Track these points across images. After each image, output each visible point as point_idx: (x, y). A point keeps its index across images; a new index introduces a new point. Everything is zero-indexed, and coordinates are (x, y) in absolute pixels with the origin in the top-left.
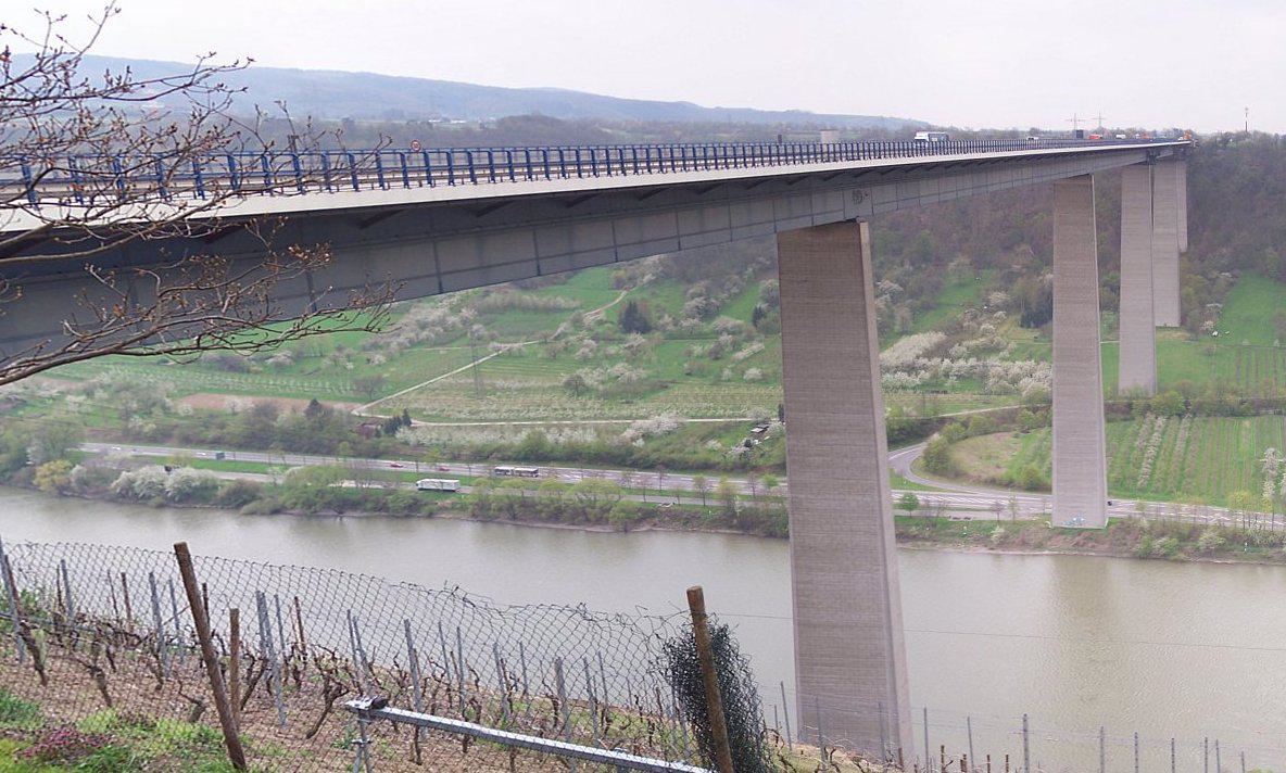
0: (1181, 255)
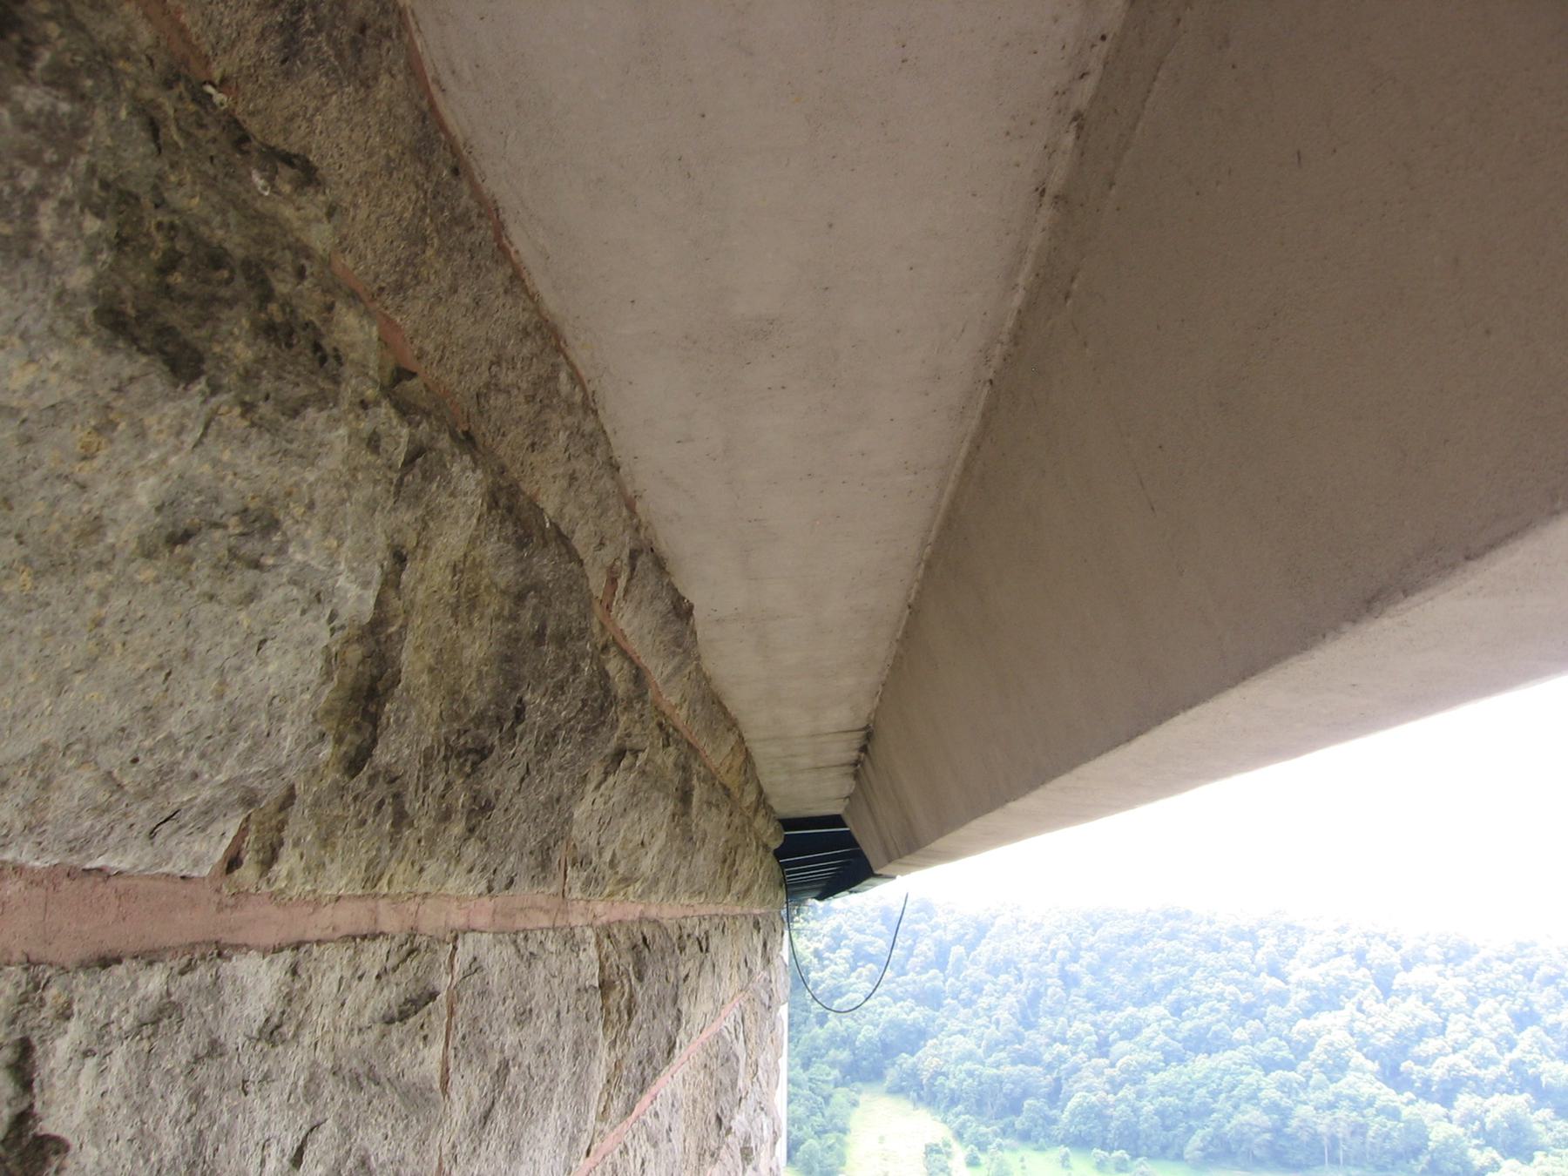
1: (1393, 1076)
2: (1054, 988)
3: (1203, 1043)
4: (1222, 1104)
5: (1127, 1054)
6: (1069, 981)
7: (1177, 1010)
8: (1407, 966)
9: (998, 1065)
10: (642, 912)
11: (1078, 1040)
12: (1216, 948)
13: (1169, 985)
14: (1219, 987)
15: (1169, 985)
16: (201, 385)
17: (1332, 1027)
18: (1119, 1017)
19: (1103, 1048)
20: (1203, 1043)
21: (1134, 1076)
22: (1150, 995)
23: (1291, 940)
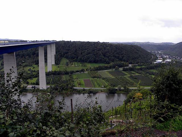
0: (55, 55)
1: (104, 56)
5: (83, 54)
19: (81, 54)
21: (84, 56)
22: (86, 49)
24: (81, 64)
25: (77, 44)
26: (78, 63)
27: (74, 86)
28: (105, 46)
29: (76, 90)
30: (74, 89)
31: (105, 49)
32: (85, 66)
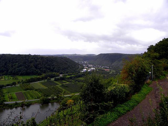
1: (36, 68)
2: (8, 62)
3: (20, 66)
4: (22, 71)
5: (14, 67)
6: (9, 61)
7: (19, 63)
8: (38, 59)
9: (2, 69)
10: (163, 70)
11: (10, 66)
12: (23, 58)
13: (18, 61)
14: (22, 61)
15: (18, 61)
16: (50, 104)
17: (32, 65)
18: (13, 64)
19: (12, 66)
20: (20, 66)
21: (15, 69)
22: (16, 62)
23: (29, 57)
24: (12, 78)
25: (7, 57)
26: (8, 76)
27: (5, 101)
28: (36, 58)
29: (7, 104)
30: (5, 104)
31: (36, 61)
32: (16, 79)
